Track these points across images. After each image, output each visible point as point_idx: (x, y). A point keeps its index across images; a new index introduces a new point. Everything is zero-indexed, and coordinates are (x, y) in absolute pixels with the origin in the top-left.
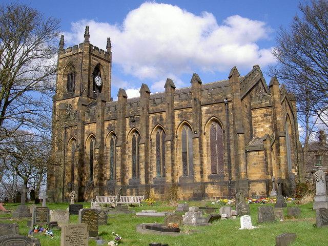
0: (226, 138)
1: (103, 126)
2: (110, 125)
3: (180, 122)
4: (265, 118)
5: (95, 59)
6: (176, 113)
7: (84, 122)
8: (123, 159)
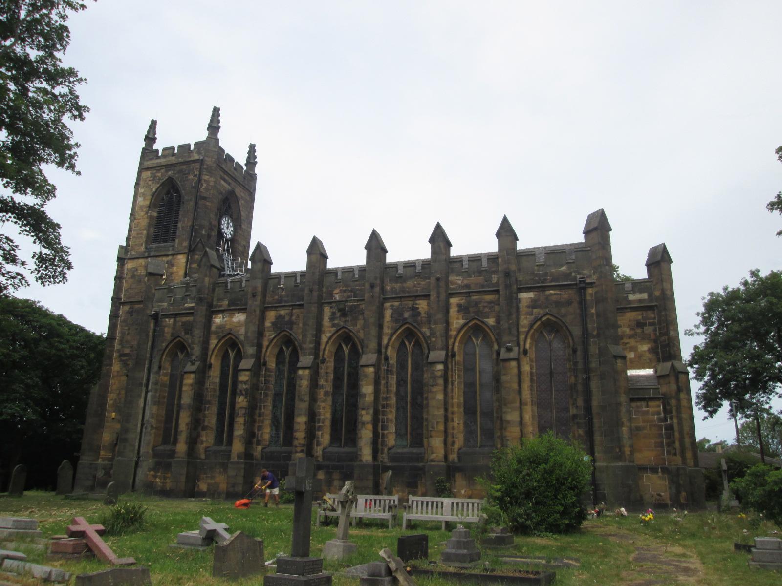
0: (580, 366)
1: (262, 319)
2: (279, 317)
3: (462, 322)
4: (639, 331)
6: (454, 301)
7: (210, 305)
8: (313, 399)
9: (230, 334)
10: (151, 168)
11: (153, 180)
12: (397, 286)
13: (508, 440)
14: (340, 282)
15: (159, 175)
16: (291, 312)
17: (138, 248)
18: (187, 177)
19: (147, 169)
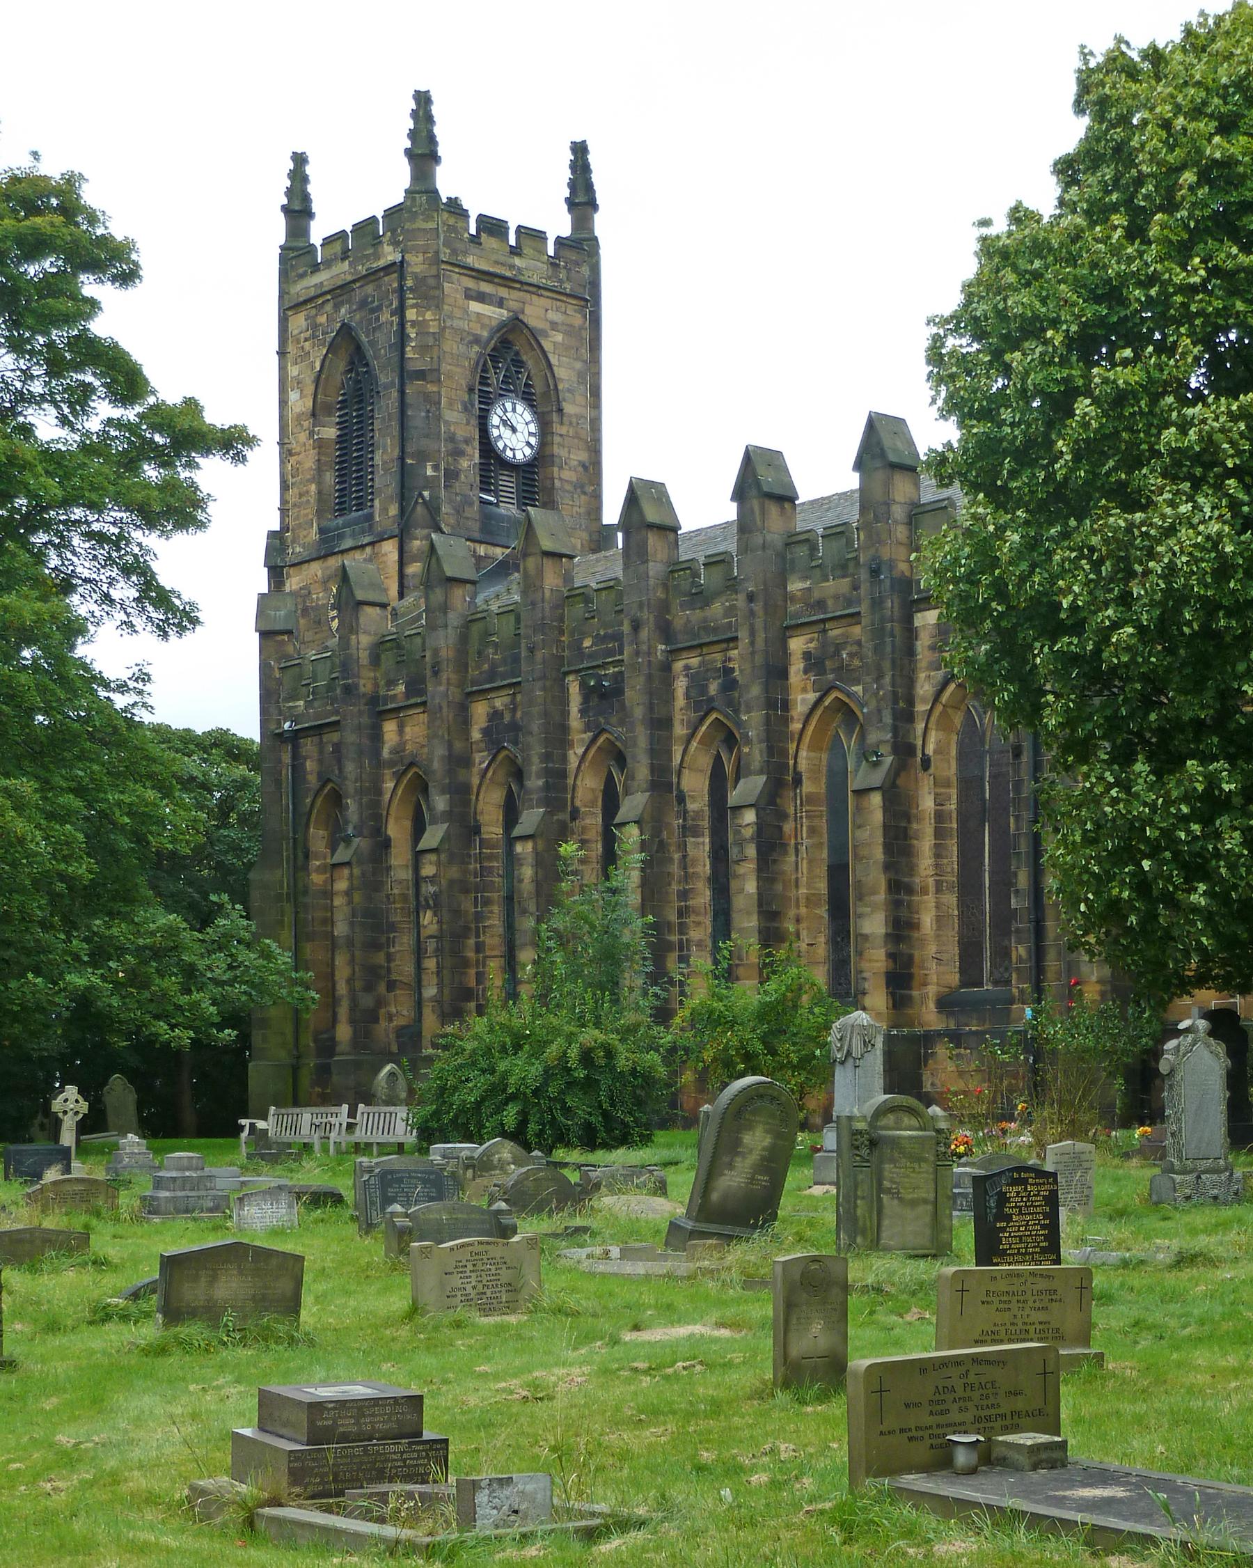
1: (465, 721)
2: (495, 715)
3: (812, 696)
5: (481, 298)
9: (412, 764)
10: (305, 302)
11: (314, 336)
12: (696, 615)
13: (864, 979)
14: (593, 617)
15: (322, 319)
16: (513, 702)
17: (305, 533)
18: (378, 319)
19: (298, 306)
